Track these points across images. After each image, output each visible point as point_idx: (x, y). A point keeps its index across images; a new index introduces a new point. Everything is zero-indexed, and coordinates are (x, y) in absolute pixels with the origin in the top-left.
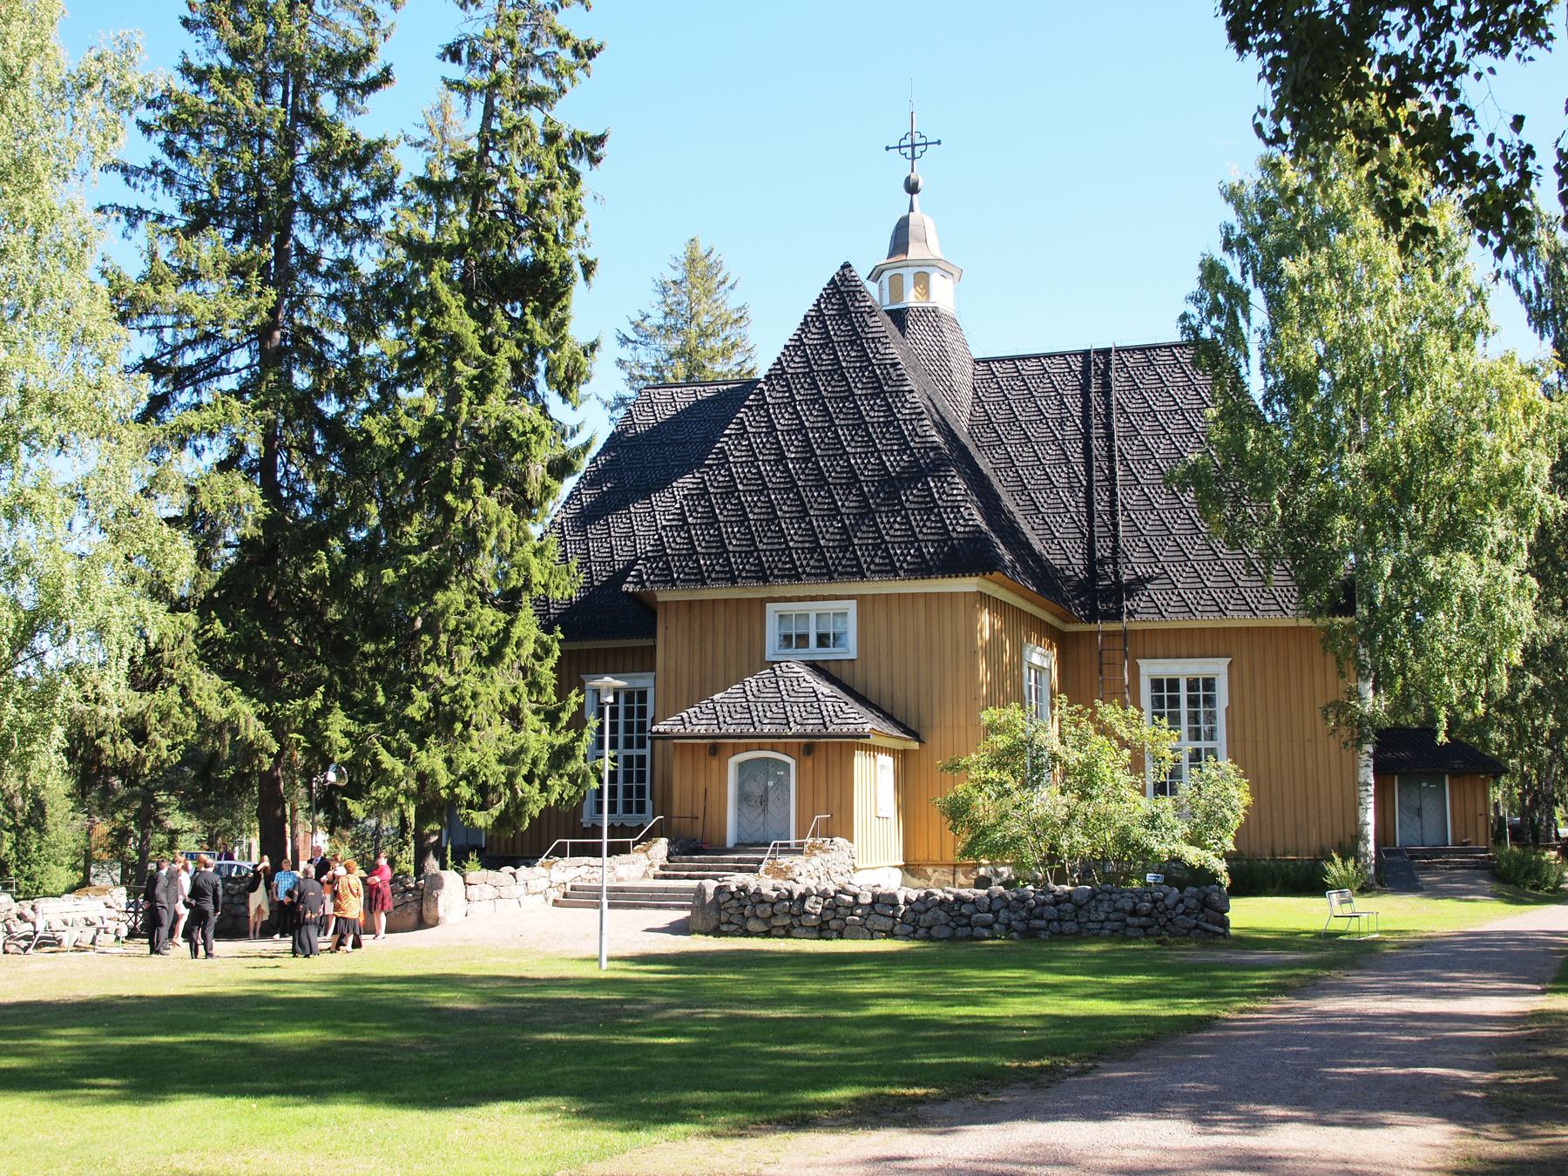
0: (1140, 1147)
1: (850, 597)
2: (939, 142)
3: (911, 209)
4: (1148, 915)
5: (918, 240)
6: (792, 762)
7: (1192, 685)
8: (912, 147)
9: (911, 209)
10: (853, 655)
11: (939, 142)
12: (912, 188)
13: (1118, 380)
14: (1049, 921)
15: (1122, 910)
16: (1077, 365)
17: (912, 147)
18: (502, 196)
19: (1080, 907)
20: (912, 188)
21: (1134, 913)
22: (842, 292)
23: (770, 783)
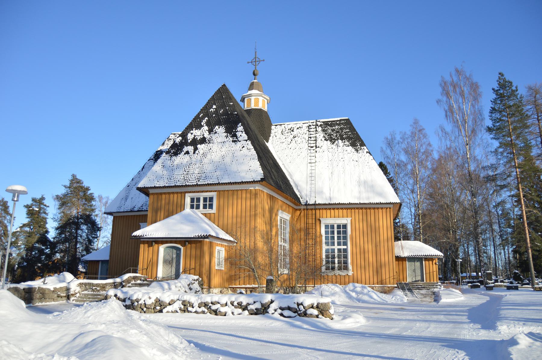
2: (264, 61)
7: (339, 227)
17: (255, 61)
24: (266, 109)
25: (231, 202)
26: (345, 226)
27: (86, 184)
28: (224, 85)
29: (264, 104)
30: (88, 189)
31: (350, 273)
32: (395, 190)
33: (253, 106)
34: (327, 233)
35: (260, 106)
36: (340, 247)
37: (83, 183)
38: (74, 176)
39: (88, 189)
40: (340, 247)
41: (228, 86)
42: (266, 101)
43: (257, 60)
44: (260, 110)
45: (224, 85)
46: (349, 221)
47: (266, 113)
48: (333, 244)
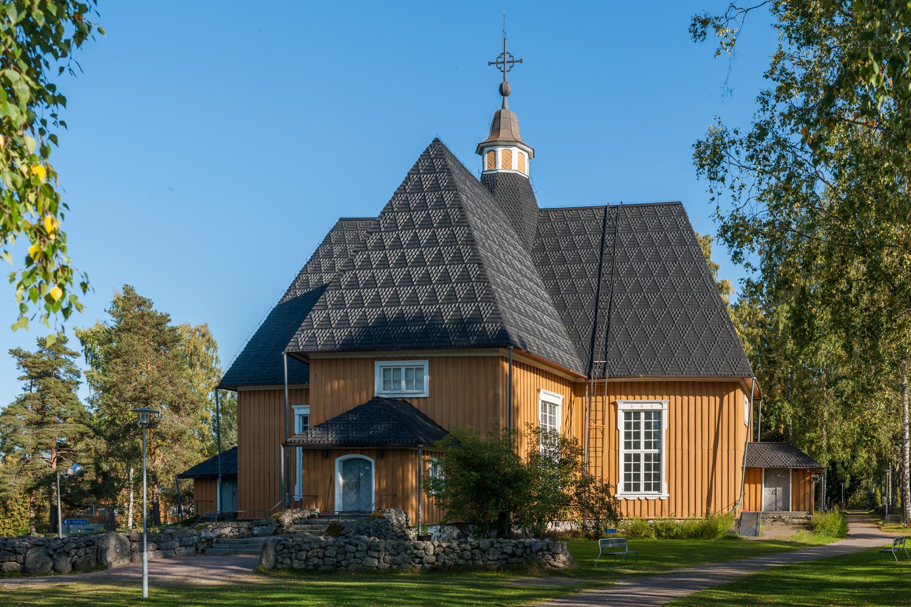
0: (905, 604)
1: (424, 358)
2: (521, 61)
3: (503, 107)
4: (521, 556)
5: (506, 128)
6: (373, 461)
7: (648, 413)
8: (504, 62)
9: (503, 107)
10: (426, 394)
11: (521, 61)
12: (503, 93)
13: (621, 225)
14: (467, 560)
15: (506, 553)
16: (600, 214)
17: (504, 62)
18: (877, 189)
19: (484, 552)
20: (503, 93)
21: (513, 555)
22: (436, 160)
23: (361, 474)
24: (526, 173)
25: (252, 402)
26: (659, 413)
27: (159, 308)
28: (437, 141)
29: (521, 163)
30: (165, 318)
31: (664, 495)
32: (384, 382)
33: (500, 168)
34: (627, 426)
35: (515, 167)
36: (637, 451)
37: (150, 306)
38: (128, 290)
39: (165, 318)
40: (637, 451)
41: (444, 141)
42: (526, 154)
43: (507, 66)
44: (514, 176)
45: (437, 141)
46: (666, 406)
47: (526, 181)
48: (637, 446)
